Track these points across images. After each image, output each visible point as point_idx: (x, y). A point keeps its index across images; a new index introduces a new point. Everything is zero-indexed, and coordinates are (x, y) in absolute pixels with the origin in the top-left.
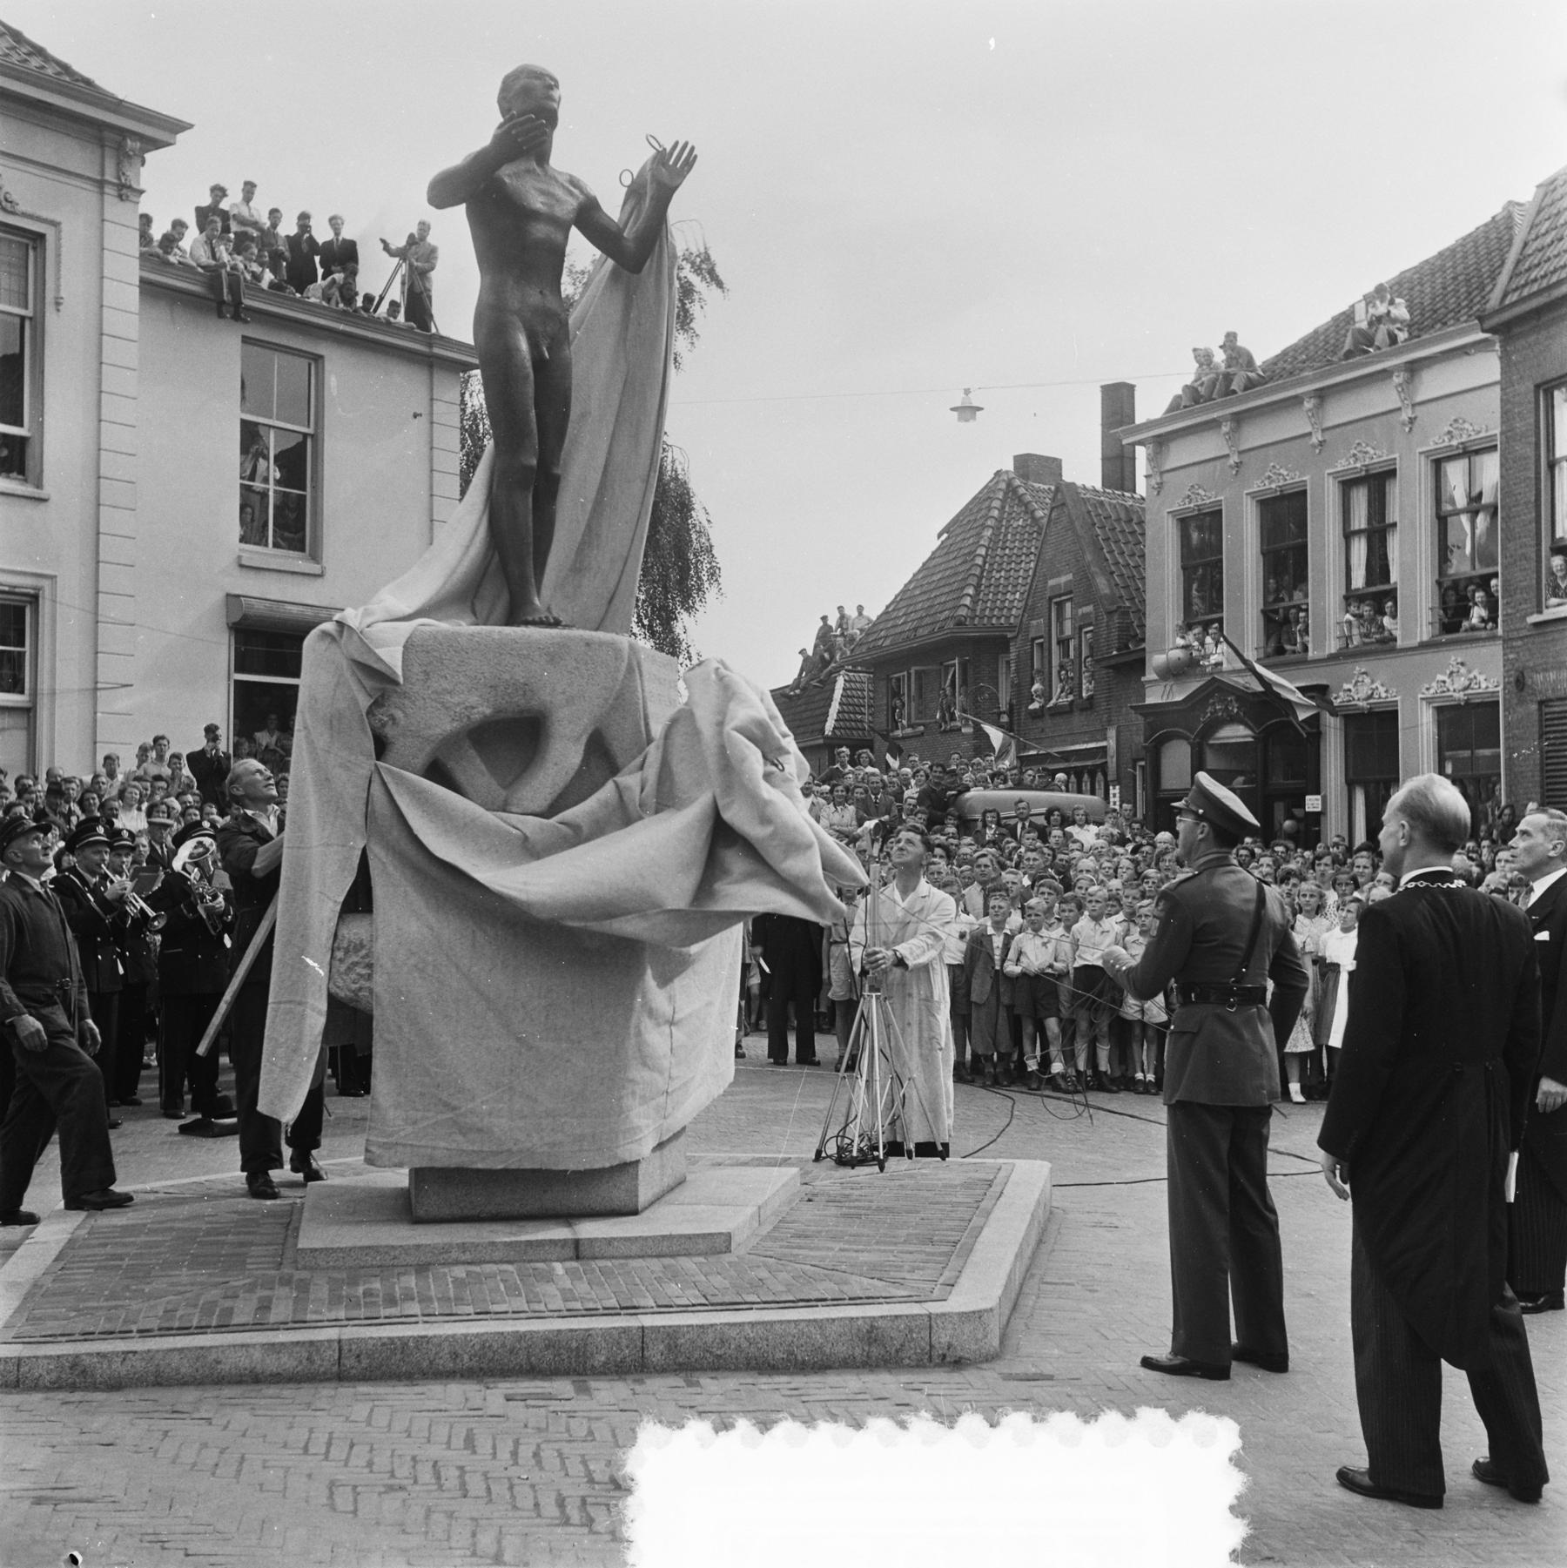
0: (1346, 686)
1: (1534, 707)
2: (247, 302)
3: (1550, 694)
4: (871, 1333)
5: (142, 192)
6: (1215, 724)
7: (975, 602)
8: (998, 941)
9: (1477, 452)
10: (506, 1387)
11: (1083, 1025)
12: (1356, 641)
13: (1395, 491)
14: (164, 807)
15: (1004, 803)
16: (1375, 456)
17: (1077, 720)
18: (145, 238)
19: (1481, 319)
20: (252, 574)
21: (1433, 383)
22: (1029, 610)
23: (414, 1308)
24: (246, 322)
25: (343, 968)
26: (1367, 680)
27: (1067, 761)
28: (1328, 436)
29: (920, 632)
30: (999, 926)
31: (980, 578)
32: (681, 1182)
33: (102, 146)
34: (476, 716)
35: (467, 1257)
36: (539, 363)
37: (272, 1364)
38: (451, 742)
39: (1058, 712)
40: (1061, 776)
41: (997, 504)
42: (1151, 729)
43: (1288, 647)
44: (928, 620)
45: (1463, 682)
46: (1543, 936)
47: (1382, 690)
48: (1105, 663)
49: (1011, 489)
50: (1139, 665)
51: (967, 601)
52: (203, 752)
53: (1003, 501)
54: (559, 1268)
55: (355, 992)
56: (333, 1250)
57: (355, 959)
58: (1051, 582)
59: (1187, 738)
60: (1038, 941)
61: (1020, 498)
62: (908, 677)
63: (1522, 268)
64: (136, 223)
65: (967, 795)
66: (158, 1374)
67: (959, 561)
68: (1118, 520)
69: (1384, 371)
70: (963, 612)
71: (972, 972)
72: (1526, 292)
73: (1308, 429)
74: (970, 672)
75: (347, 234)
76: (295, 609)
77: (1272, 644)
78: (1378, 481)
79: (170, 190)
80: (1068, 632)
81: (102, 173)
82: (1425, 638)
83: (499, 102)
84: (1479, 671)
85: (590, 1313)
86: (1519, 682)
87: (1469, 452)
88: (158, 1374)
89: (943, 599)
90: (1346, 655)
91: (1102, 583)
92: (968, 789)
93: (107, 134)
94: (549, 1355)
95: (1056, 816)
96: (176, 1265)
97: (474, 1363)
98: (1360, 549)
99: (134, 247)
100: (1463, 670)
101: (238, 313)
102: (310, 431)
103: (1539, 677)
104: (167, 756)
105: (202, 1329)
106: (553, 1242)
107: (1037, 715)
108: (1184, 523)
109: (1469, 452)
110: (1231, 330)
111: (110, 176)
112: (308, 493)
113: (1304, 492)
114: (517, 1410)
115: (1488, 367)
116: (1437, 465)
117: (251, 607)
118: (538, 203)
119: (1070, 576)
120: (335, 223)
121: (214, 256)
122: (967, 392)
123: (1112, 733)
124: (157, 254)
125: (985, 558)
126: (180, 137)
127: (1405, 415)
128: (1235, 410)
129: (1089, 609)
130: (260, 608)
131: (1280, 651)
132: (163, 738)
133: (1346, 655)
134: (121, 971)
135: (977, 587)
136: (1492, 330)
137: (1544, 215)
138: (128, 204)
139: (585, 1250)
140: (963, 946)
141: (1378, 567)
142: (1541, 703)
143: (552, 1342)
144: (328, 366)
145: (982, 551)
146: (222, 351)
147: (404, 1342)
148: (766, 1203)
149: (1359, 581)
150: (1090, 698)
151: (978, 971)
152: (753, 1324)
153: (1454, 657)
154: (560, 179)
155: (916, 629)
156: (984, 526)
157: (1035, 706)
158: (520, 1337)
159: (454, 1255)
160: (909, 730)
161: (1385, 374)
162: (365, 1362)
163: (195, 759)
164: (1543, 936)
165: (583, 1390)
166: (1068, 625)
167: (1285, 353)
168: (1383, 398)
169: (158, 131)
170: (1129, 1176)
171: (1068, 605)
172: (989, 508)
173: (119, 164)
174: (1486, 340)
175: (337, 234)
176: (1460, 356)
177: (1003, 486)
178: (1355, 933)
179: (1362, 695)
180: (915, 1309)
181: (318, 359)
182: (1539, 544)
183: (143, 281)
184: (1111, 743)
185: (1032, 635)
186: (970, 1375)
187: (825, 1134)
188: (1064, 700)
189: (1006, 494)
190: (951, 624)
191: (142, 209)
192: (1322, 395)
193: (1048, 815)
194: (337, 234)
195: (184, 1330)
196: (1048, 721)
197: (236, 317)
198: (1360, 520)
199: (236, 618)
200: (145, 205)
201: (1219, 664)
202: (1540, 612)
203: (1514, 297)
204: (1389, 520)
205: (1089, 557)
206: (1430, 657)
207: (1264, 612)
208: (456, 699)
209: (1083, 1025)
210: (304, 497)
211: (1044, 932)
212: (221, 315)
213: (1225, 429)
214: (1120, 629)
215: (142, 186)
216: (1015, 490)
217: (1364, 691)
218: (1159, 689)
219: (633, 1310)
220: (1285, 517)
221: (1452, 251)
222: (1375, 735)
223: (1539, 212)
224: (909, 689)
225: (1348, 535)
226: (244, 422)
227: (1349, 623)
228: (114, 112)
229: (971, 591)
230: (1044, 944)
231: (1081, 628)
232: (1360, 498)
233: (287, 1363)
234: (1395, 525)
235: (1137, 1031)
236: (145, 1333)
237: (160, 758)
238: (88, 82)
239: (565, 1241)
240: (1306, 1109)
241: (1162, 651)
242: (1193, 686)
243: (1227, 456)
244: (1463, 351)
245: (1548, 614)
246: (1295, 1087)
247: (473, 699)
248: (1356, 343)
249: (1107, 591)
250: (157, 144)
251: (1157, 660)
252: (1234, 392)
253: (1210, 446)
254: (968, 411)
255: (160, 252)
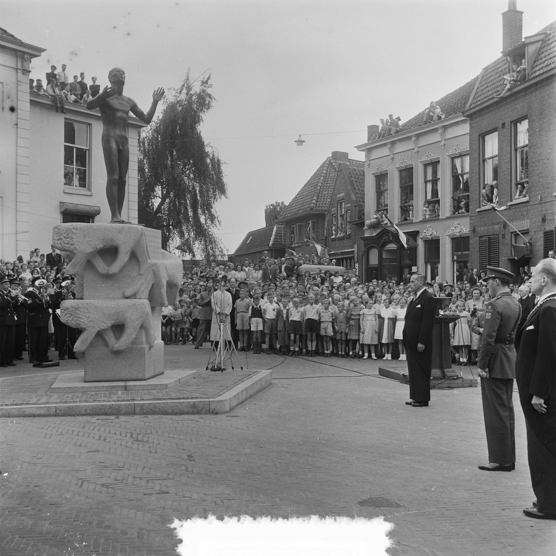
0: (425, 231)
1: (478, 238)
2: (66, 107)
3: (482, 234)
4: (194, 406)
5: (30, 72)
6: (386, 243)
7: (317, 202)
8: (285, 312)
9: (464, 155)
10: (98, 417)
11: (309, 337)
12: (427, 217)
13: (440, 167)
14: (36, 271)
15: (313, 270)
16: (433, 156)
17: (346, 241)
18: (31, 87)
19: (463, 113)
20: (68, 195)
21: (451, 133)
22: (331, 205)
23: (78, 400)
24: (65, 113)
25: (64, 314)
26: (431, 229)
27: (343, 255)
28: (420, 149)
29: (300, 212)
30: (285, 307)
31: (319, 194)
32: (163, 373)
33: (17, 57)
34: (99, 247)
35: (96, 390)
36: (119, 151)
37: (38, 412)
38: (92, 254)
39: (340, 239)
40: (334, 261)
41: (325, 168)
42: (366, 245)
43: (408, 218)
44: (302, 208)
45: (458, 230)
46: (419, 306)
47: (435, 232)
48: (354, 223)
49: (330, 163)
50: (363, 224)
51: (314, 201)
52: (51, 253)
53: (328, 167)
54: (120, 392)
55: (67, 321)
56: (60, 388)
57: (67, 312)
58: (338, 196)
59: (377, 248)
60: (297, 311)
61: (333, 166)
62: (296, 227)
63: (477, 96)
64: (28, 82)
65: (301, 267)
66: (9, 414)
67: (312, 188)
68: (360, 175)
69: (436, 129)
70: (312, 205)
71: (278, 321)
72: (477, 104)
73: (389, 154)
74: (315, 225)
75: (97, 83)
76: (82, 206)
77: (403, 217)
78: (435, 164)
79: (38, 70)
80: (343, 212)
81: (17, 66)
82: (448, 216)
83: (109, 77)
84: (462, 227)
85: (123, 401)
86: (474, 230)
87: (461, 156)
88: (9, 414)
89: (307, 201)
90: (424, 221)
91: (353, 197)
92: (301, 265)
93: (19, 53)
94: (110, 410)
95: (328, 274)
96: (20, 392)
97: (91, 412)
98: (429, 186)
99: (28, 90)
100: (459, 226)
101: (63, 110)
102: (88, 148)
103: (479, 229)
104: (40, 255)
105: (21, 404)
106: (119, 386)
107: (334, 240)
108: (401, 171)
109: (461, 156)
110: (391, 114)
111: (19, 66)
112: (87, 169)
113: (413, 167)
114: (99, 422)
115: (465, 129)
116: (453, 159)
117: (68, 206)
118: (118, 106)
119: (344, 194)
120: (94, 79)
121: (54, 92)
122: (300, 136)
123: (356, 246)
124: (35, 90)
125: (321, 187)
126: (42, 53)
127: (442, 143)
128: (367, 147)
129: (349, 205)
130: (70, 207)
131: (406, 219)
132: (37, 249)
133: (424, 221)
134: (16, 319)
135: (318, 197)
136: (467, 116)
137: (484, 79)
138: (25, 76)
139: (128, 388)
140: (275, 313)
141: (435, 193)
142: (480, 237)
143: (111, 407)
144: (94, 128)
145: (320, 185)
146: (56, 125)
147: (73, 407)
148: (182, 378)
149: (429, 197)
150: (350, 234)
151: (280, 320)
152: (163, 403)
153: (456, 222)
154: (125, 99)
155: (298, 211)
156: (321, 176)
157: (333, 237)
158: (103, 406)
159: (93, 389)
160: (297, 245)
161: (436, 130)
162: (62, 412)
163: (49, 256)
164: (419, 306)
165: (118, 418)
166: (343, 210)
167: (409, 121)
168: (435, 138)
169: (36, 52)
170: (304, 376)
171: (343, 203)
172: (323, 170)
173: (22, 63)
174: (464, 120)
175: (94, 83)
176: (456, 125)
177: (328, 162)
178: (406, 309)
179: (429, 234)
180: (207, 400)
181: (90, 125)
182: (480, 186)
183: (31, 100)
184: (355, 249)
185: (333, 213)
186: (219, 416)
187: (209, 361)
188: (342, 235)
189: (329, 165)
190: (309, 209)
191: (30, 77)
192: (393, 143)
193: (325, 273)
194: (94, 83)
195: (17, 404)
196: (337, 242)
197: (62, 112)
198: (430, 177)
199: (63, 210)
200: (31, 76)
201: (387, 224)
202: (480, 208)
203: (473, 106)
204: (438, 177)
205: (349, 188)
206: (449, 222)
207: (401, 207)
208: (93, 243)
209: (309, 337)
210: (86, 170)
211: (299, 309)
212: (57, 112)
213: (440, 132)
214: (359, 212)
215: (30, 70)
216: (332, 164)
217: (430, 233)
218: (369, 231)
219: (134, 400)
220: (407, 174)
221: (463, 87)
222: (433, 246)
223: (483, 77)
224: (296, 231)
225: (426, 182)
226: (65, 146)
227: (426, 210)
228: (21, 46)
229: (315, 198)
230: (298, 312)
231: (347, 211)
232: (430, 170)
233: (42, 412)
234: (439, 179)
235: (325, 339)
236: (6, 405)
237: (37, 255)
238: (12, 36)
239: (122, 386)
240: (377, 362)
241: (370, 219)
242: (378, 231)
243: (389, 155)
244: (457, 123)
245: (483, 208)
246: (373, 355)
247: (97, 243)
248: (427, 119)
249: (355, 199)
250: (36, 56)
251: (367, 222)
252: (392, 134)
253: (385, 151)
254: (300, 142)
255: (36, 91)
